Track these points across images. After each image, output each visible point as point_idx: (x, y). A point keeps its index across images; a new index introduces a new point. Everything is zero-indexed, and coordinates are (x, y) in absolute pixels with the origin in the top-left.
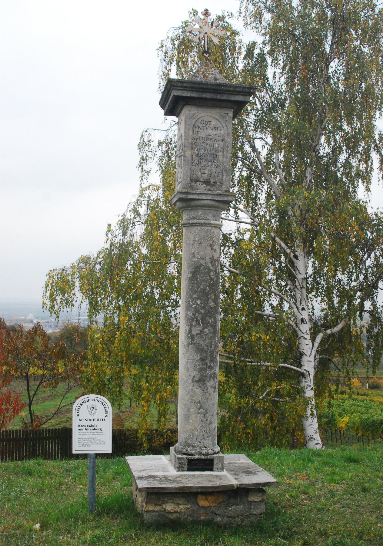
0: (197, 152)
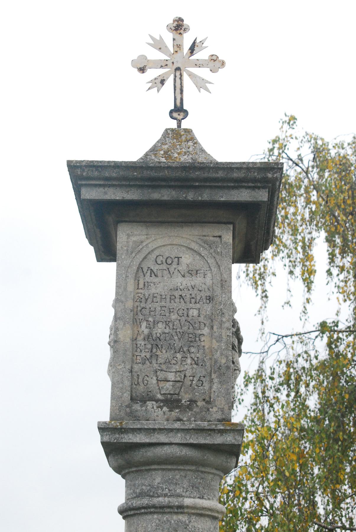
0: (146, 331)
